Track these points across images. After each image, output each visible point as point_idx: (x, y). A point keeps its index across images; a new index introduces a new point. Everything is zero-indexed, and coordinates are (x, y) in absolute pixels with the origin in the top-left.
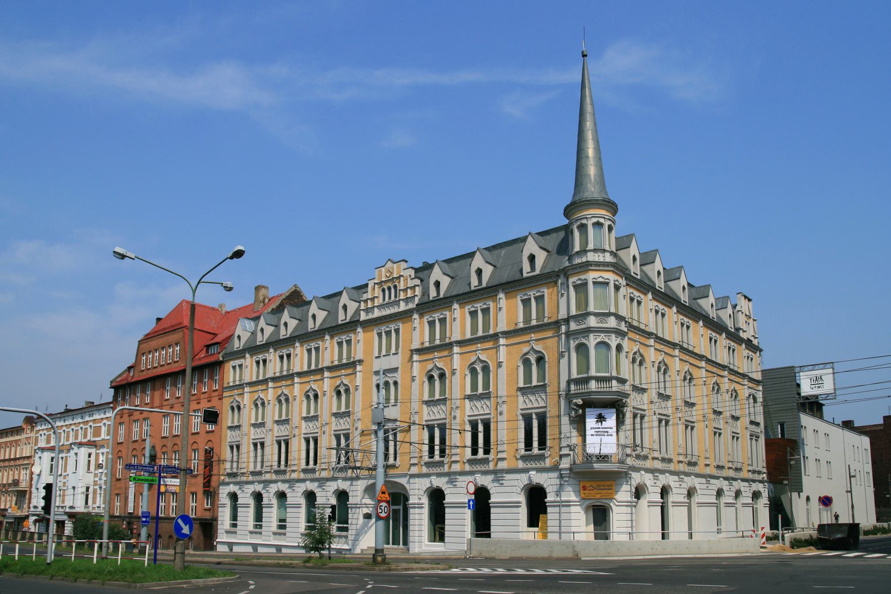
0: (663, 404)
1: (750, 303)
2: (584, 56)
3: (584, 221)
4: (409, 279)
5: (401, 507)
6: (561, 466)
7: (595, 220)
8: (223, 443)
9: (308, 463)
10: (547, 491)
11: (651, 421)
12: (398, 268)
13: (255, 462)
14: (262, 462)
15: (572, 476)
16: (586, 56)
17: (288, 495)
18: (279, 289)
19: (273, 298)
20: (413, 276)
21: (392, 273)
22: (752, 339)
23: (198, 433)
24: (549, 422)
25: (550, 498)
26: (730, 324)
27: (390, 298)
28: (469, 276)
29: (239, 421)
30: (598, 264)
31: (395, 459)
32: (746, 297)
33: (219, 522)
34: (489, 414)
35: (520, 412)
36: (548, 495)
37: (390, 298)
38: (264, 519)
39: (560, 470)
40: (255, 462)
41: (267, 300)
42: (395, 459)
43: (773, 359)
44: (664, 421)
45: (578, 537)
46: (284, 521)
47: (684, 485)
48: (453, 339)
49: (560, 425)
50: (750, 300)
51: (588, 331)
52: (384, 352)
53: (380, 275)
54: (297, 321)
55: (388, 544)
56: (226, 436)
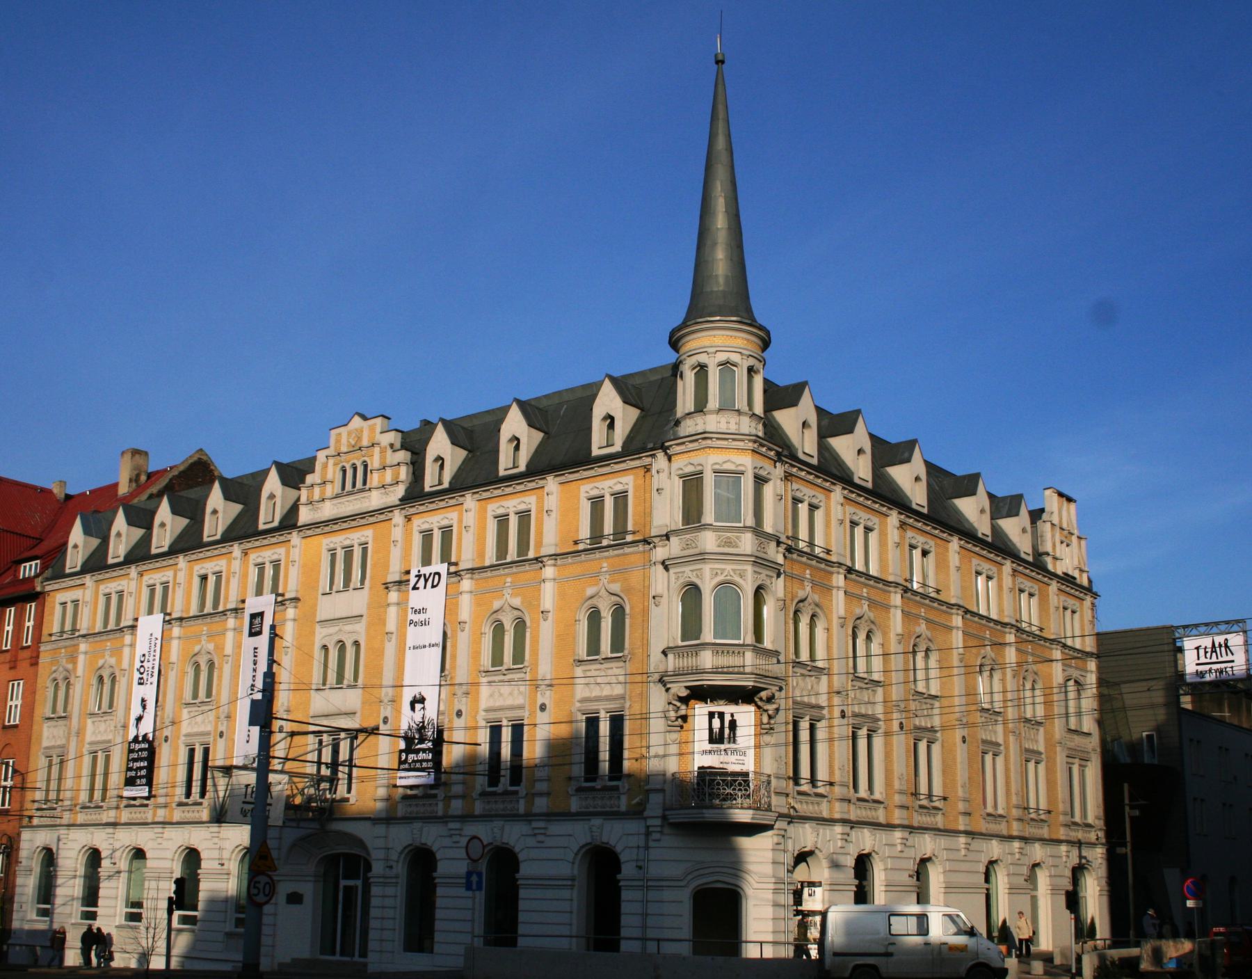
0: (865, 696)
1: (1073, 506)
2: (720, 62)
3: (703, 358)
4: (389, 451)
5: (359, 883)
6: (646, 814)
7: (722, 357)
8: (34, 748)
9: (188, 794)
10: (623, 858)
11: (832, 732)
12: (372, 429)
13: (92, 790)
14: (105, 790)
15: (667, 830)
16: (723, 62)
17: (148, 855)
18: (169, 456)
19: (158, 472)
20: (398, 445)
21: (359, 439)
22: (1076, 574)
23: (16, 726)
24: (627, 726)
25: (627, 870)
26: (1024, 545)
27: (354, 485)
28: (589, 429)
29: (65, 711)
30: (723, 436)
31: (349, 791)
32: (1061, 495)
33: (16, 906)
34: (521, 707)
35: (578, 705)
36: (623, 867)
37: (354, 485)
38: (100, 902)
39: (645, 819)
40: (92, 790)
41: (143, 478)
42: (349, 791)
43: (1126, 613)
44: (862, 727)
45: (668, 948)
46: (139, 905)
47: (910, 853)
48: (545, 551)
49: (1067, 700)
50: (1069, 500)
51: (702, 557)
52: (512, 554)
53: (338, 441)
54: (542, 435)
55: (334, 953)
56: (40, 735)
